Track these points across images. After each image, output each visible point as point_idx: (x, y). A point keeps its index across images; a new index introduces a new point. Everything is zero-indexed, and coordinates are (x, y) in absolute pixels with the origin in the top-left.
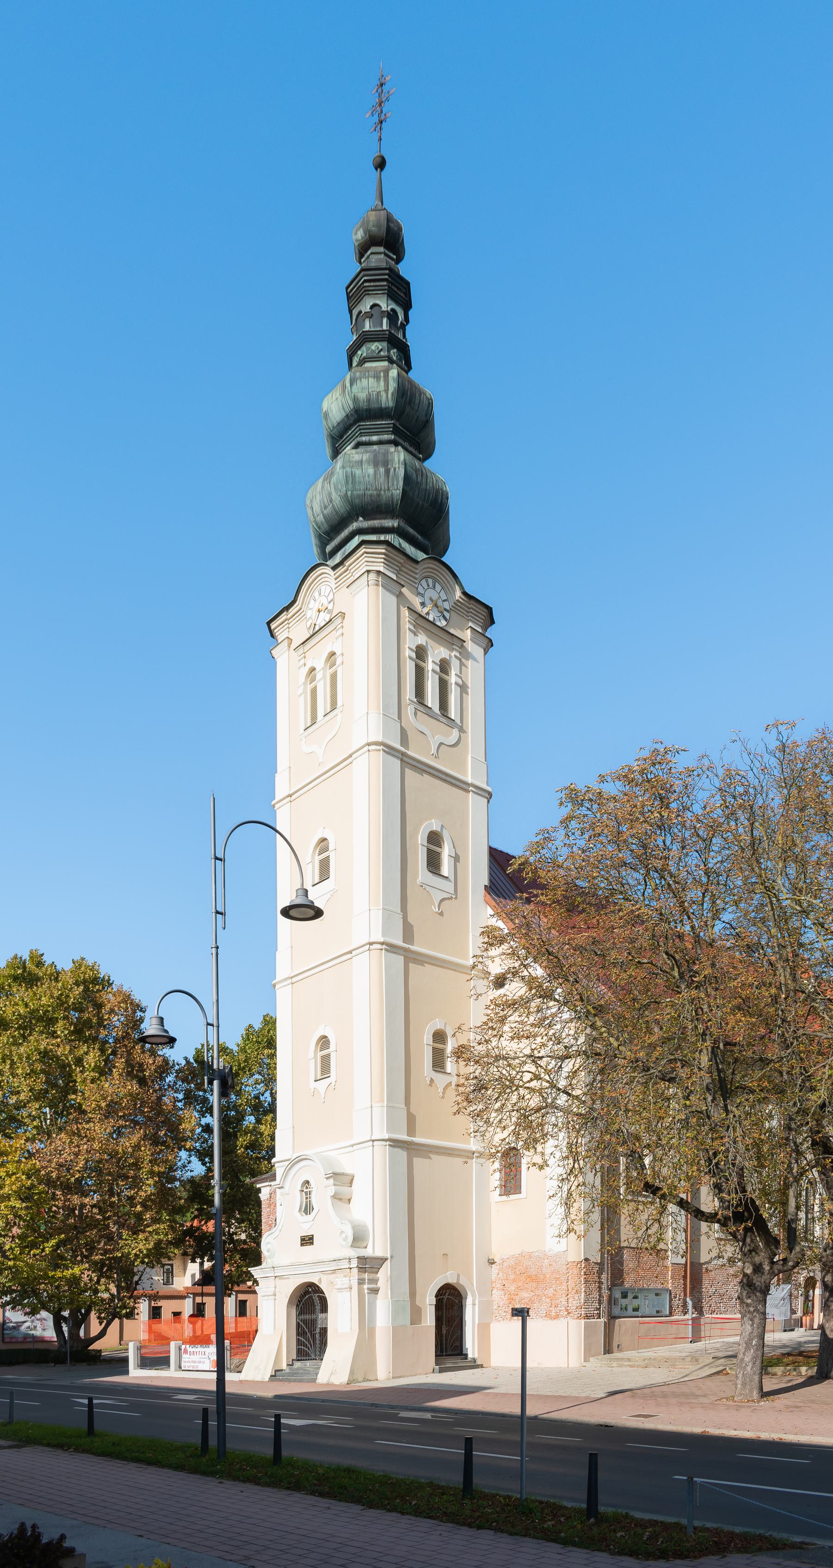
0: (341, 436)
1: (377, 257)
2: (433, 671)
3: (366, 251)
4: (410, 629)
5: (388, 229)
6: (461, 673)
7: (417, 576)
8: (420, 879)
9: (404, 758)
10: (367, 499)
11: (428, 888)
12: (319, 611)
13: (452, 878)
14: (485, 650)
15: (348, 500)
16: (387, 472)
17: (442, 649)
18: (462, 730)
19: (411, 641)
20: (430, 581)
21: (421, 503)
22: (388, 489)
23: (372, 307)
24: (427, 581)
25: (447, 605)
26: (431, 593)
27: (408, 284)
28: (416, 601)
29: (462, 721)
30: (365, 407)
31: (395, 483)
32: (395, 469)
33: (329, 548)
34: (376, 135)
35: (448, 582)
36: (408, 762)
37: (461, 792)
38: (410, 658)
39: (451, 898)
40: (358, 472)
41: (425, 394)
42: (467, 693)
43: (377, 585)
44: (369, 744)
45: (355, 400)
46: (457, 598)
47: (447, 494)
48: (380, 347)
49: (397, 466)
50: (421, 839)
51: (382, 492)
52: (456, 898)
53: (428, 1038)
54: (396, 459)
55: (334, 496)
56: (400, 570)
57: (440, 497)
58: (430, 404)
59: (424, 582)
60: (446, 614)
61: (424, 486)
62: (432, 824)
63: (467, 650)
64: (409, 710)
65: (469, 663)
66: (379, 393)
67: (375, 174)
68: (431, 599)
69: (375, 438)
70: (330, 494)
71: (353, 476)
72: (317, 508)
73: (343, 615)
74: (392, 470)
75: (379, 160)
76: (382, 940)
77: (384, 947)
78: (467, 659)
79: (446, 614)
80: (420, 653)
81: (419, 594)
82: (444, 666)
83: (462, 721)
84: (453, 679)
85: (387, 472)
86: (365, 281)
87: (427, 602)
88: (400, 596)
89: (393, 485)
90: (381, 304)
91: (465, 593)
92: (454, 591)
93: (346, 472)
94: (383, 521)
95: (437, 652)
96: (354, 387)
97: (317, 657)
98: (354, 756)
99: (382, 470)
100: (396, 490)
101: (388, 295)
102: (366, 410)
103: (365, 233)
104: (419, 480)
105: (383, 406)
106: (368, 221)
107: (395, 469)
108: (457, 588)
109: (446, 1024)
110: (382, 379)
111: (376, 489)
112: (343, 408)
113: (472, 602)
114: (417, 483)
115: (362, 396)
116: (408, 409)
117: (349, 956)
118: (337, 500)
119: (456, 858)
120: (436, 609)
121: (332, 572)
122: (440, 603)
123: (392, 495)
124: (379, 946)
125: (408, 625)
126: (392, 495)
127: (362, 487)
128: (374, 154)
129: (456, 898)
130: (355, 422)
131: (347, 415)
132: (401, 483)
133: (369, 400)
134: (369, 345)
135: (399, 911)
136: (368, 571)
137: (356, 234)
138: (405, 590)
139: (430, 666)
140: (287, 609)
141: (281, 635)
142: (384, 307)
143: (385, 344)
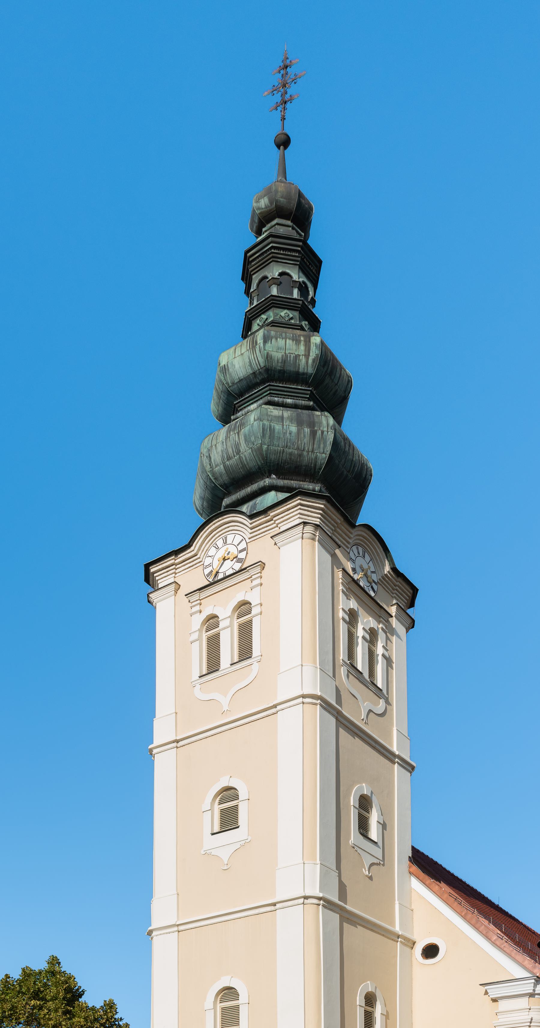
0: (241, 394)
1: (282, 227)
2: (364, 638)
3: (269, 221)
4: (343, 591)
5: (299, 204)
6: (386, 645)
7: (351, 541)
8: (352, 841)
9: (340, 718)
10: (285, 457)
11: (359, 850)
12: (224, 559)
13: (380, 844)
14: (406, 629)
15: (262, 454)
16: (313, 434)
17: (371, 619)
18: (388, 702)
19: (346, 603)
20: (360, 549)
21: (345, 473)
22: (313, 451)
23: (281, 274)
24: (357, 548)
25: (374, 577)
26: (360, 561)
27: (320, 262)
28: (349, 566)
29: (388, 694)
30: (279, 368)
31: (322, 446)
32: (323, 432)
33: (226, 501)
34: (278, 114)
35: (378, 555)
36: (343, 722)
37: (387, 762)
38: (344, 619)
39: (379, 864)
40: (278, 427)
41: (345, 370)
42: (392, 668)
43: (313, 539)
44: (304, 696)
45: (268, 357)
46: (386, 572)
47: (371, 471)
48: (291, 316)
49: (325, 429)
50: (353, 801)
51: (305, 453)
52: (383, 865)
53: (360, 1000)
54: (324, 422)
55: (243, 447)
56: (335, 531)
57: (365, 473)
58: (349, 382)
59: (354, 548)
60: (374, 585)
61: (350, 457)
62: (362, 787)
63: (392, 626)
64: (343, 671)
65: (394, 639)
66: (297, 356)
67: (276, 153)
68: (361, 567)
69: (289, 401)
70: (237, 446)
71: (272, 430)
72: (216, 457)
73: (262, 565)
74: (319, 433)
75: (283, 137)
76: (321, 895)
77: (322, 902)
78: (393, 635)
79: (374, 585)
80: (352, 617)
81: (350, 559)
82: (373, 634)
83: (388, 694)
84: (380, 650)
85: (313, 434)
86: (273, 247)
87: (358, 569)
88: (334, 556)
89: (319, 447)
90: (292, 274)
91: (394, 569)
92: (384, 565)
93: (264, 425)
94: (301, 483)
95: (366, 621)
96: (268, 345)
97: (222, 605)
98: (279, 707)
99: (307, 430)
100: (322, 454)
101: (300, 268)
102: (280, 371)
103: (271, 202)
104: (347, 449)
105: (301, 370)
106: (276, 191)
107: (323, 432)
108: (387, 563)
109: (376, 988)
110: (302, 343)
111: (298, 449)
112: (250, 365)
113: (399, 579)
114: (345, 452)
115: (278, 355)
116: (327, 380)
117: (272, 908)
118: (246, 451)
119: (384, 826)
120: (365, 578)
121: (247, 521)
122: (369, 573)
123: (316, 458)
124: (316, 901)
125: (341, 587)
126: (316, 458)
127: (282, 443)
128: (275, 130)
129: (383, 865)
130: (263, 382)
131: (254, 373)
132: (329, 448)
133: (284, 361)
134: (277, 311)
135: (335, 868)
136: (305, 523)
137: (257, 202)
138: (338, 552)
139: (360, 632)
140: (176, 553)
141: (163, 580)
142: (295, 277)
143: (296, 314)
